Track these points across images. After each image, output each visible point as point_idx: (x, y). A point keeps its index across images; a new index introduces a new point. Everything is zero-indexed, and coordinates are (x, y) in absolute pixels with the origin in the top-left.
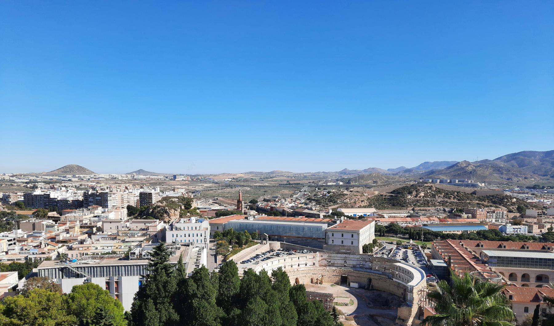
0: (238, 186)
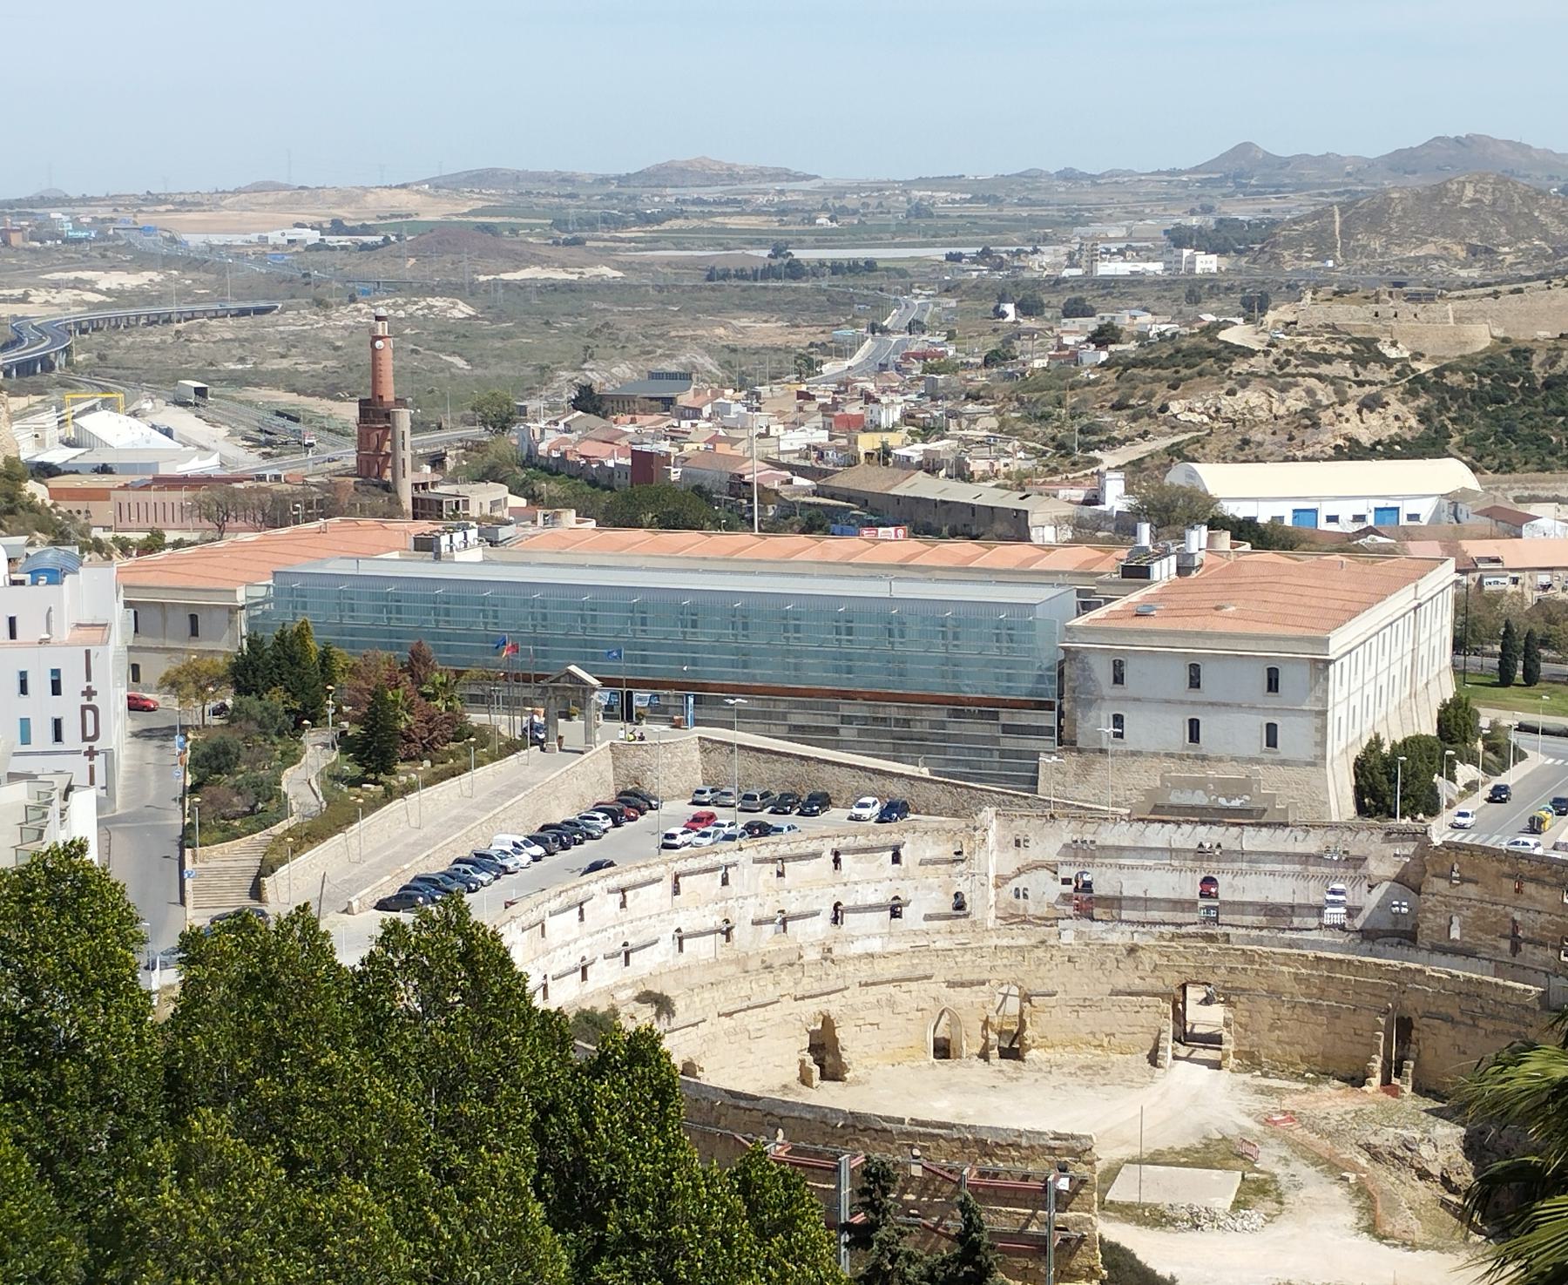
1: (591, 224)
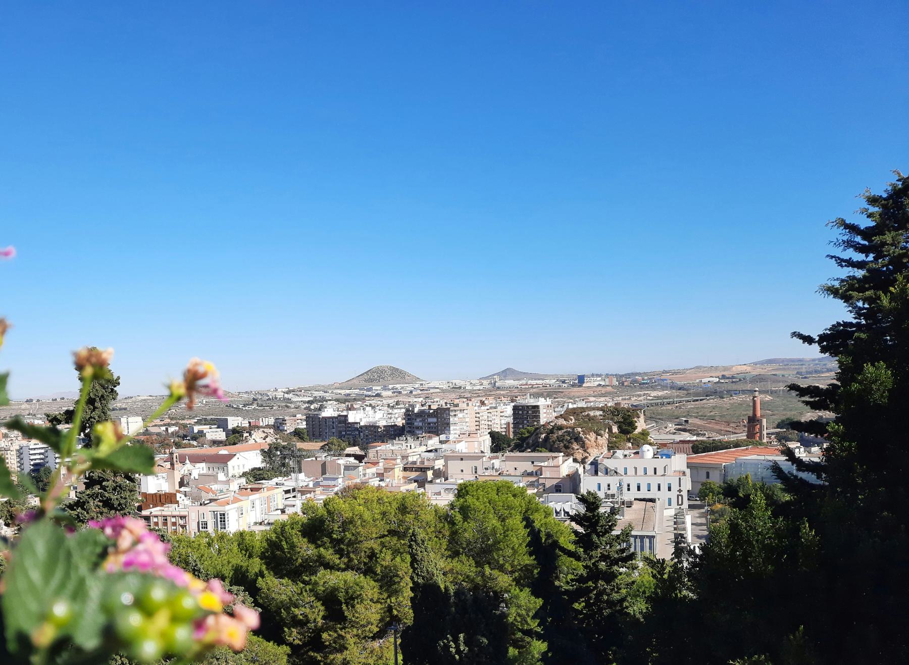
0: (737, 392)
1: (811, 373)
